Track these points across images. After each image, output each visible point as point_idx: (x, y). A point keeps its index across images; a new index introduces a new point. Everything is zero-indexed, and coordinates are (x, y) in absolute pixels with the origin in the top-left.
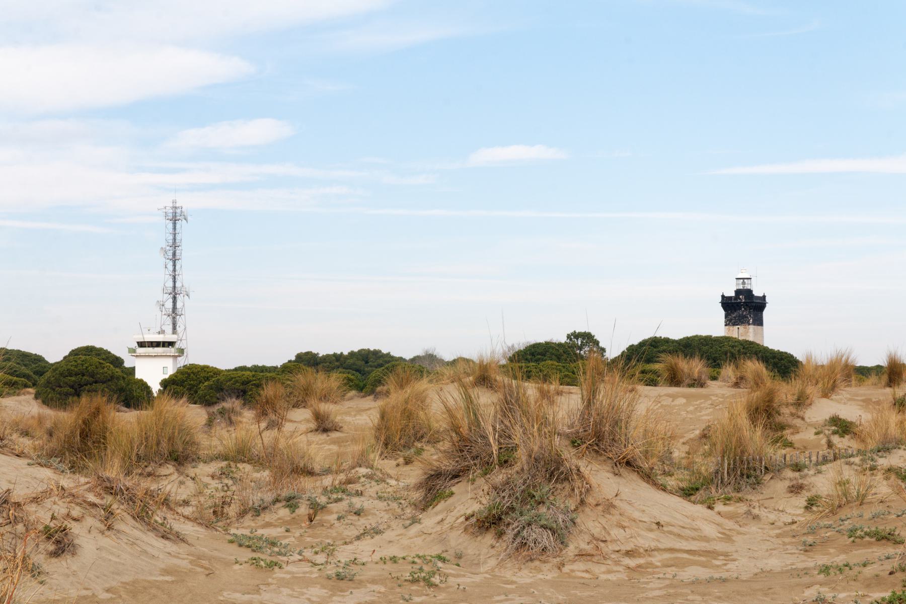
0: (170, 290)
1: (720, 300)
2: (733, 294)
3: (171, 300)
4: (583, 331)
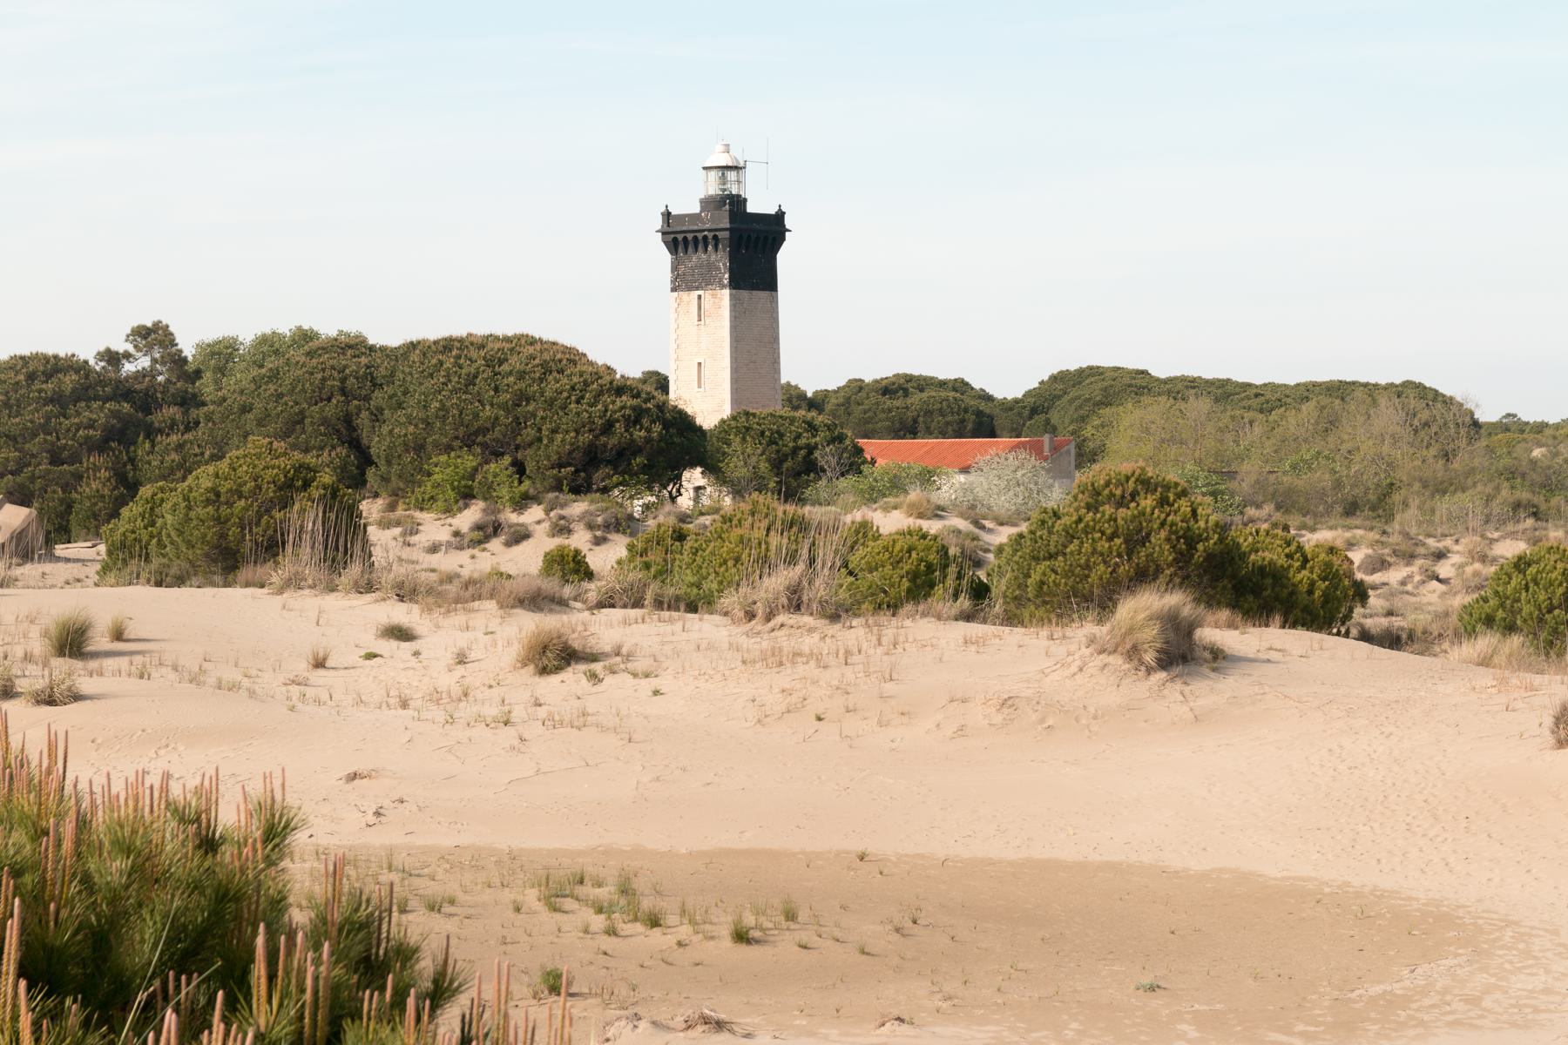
2: (696, 209)
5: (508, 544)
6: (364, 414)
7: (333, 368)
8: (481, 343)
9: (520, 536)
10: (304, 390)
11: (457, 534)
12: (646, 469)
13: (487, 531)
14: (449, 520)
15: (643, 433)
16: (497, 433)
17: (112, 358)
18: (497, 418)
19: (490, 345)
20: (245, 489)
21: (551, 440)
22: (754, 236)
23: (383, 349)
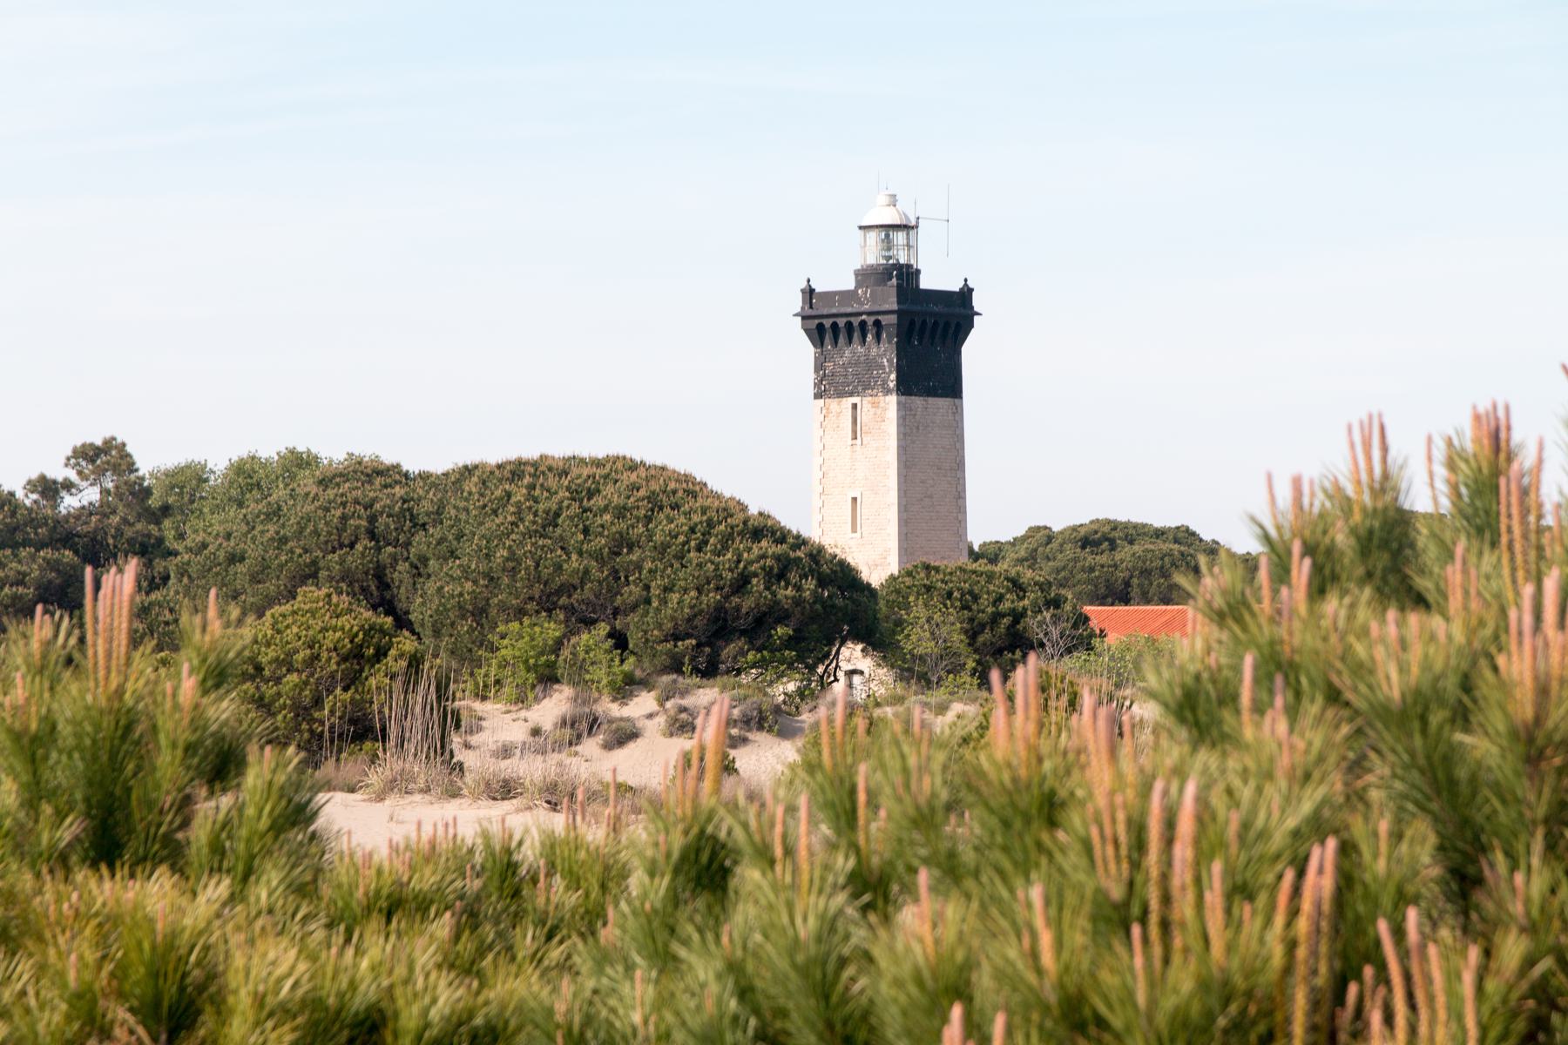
1: (797, 303)
2: (849, 284)
5: (608, 747)
6: (403, 567)
7: (357, 502)
8: (562, 469)
9: (624, 736)
10: (316, 533)
11: (536, 732)
12: (790, 642)
13: (580, 726)
14: (523, 714)
15: (790, 592)
16: (588, 592)
17: (48, 489)
18: (587, 571)
19: (575, 471)
20: (300, 657)
21: (664, 602)
22: (930, 321)
23: (425, 476)
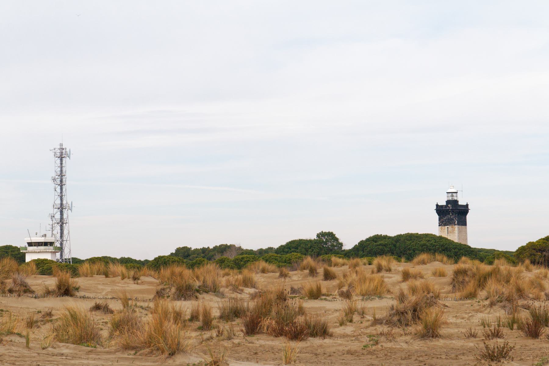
0: (59, 206)
1: (435, 208)
2: (445, 204)
3: (59, 213)
4: (327, 231)
